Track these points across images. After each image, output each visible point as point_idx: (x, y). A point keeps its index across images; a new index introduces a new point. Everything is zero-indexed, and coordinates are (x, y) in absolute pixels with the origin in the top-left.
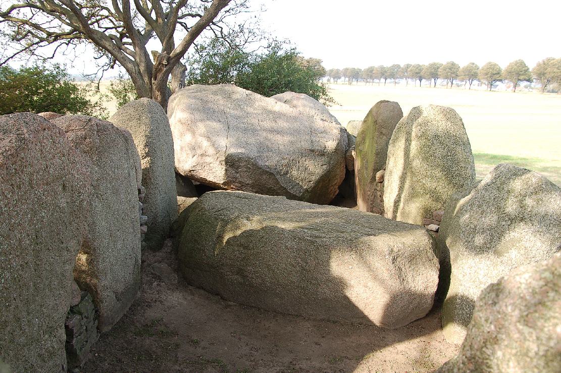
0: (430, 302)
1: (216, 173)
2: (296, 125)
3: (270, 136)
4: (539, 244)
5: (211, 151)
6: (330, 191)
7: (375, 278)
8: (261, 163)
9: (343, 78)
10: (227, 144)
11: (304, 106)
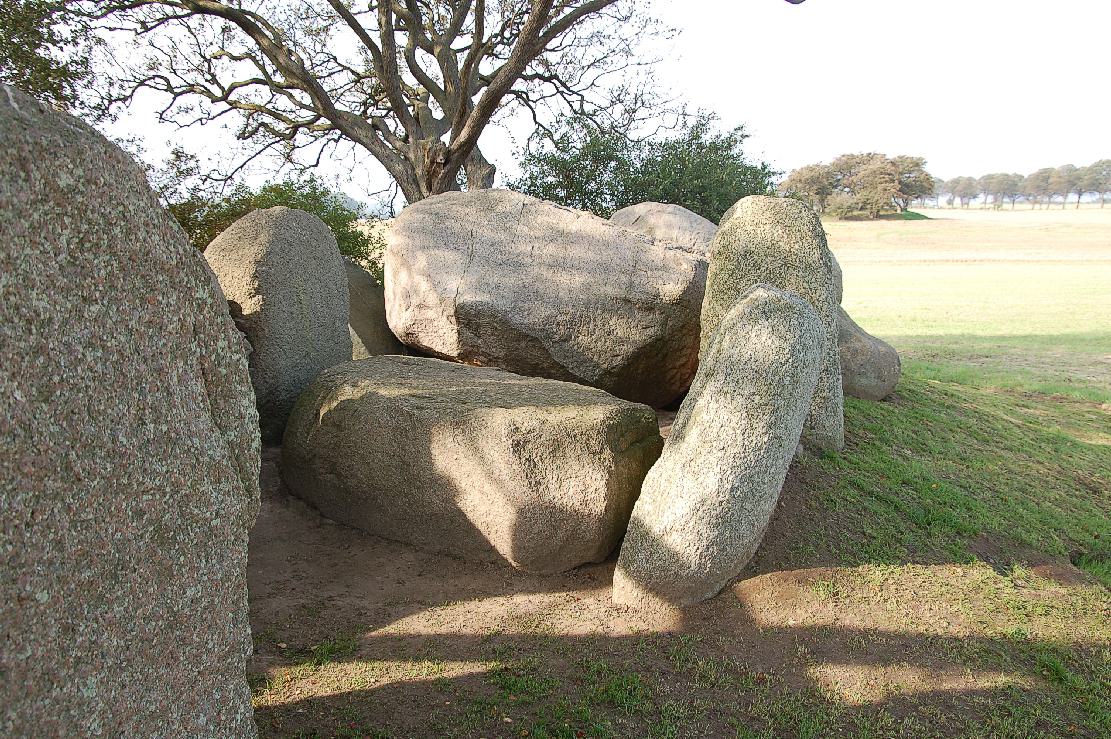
0: (591, 531)
1: (443, 337)
2: (607, 255)
3: (547, 274)
4: (724, 414)
5: (432, 299)
6: (669, 377)
7: (490, 475)
8: (517, 319)
9: (982, 197)
10: (462, 287)
11: (669, 226)
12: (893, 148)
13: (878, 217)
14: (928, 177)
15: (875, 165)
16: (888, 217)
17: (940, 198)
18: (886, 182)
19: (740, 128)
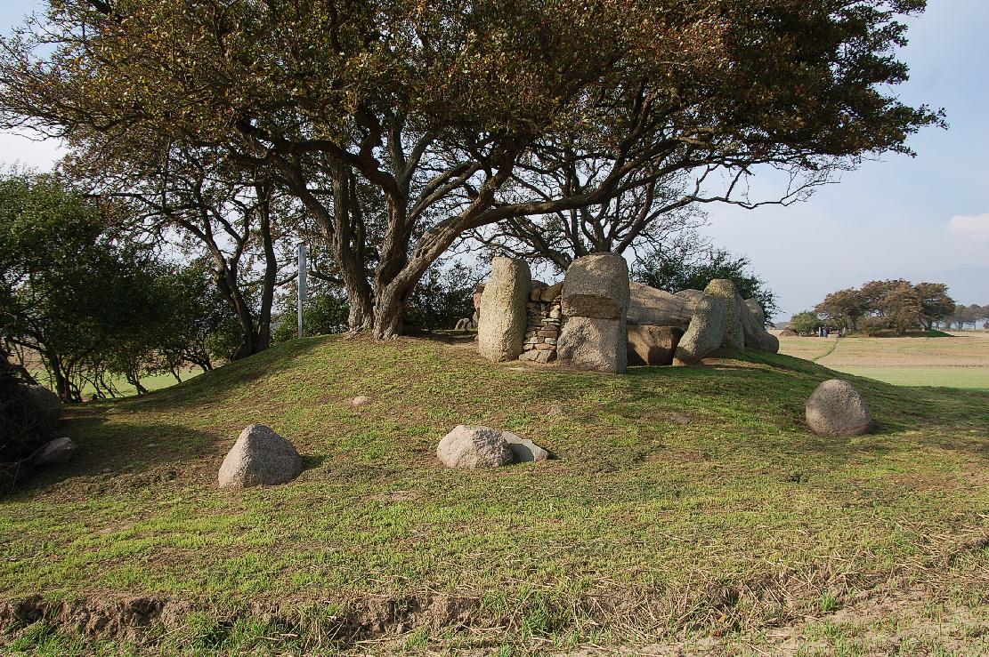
7: (643, 340)
12: (916, 275)
13: (904, 334)
14: (950, 301)
15: (898, 291)
16: (913, 335)
17: (977, 323)
18: (910, 304)
19: (742, 260)
